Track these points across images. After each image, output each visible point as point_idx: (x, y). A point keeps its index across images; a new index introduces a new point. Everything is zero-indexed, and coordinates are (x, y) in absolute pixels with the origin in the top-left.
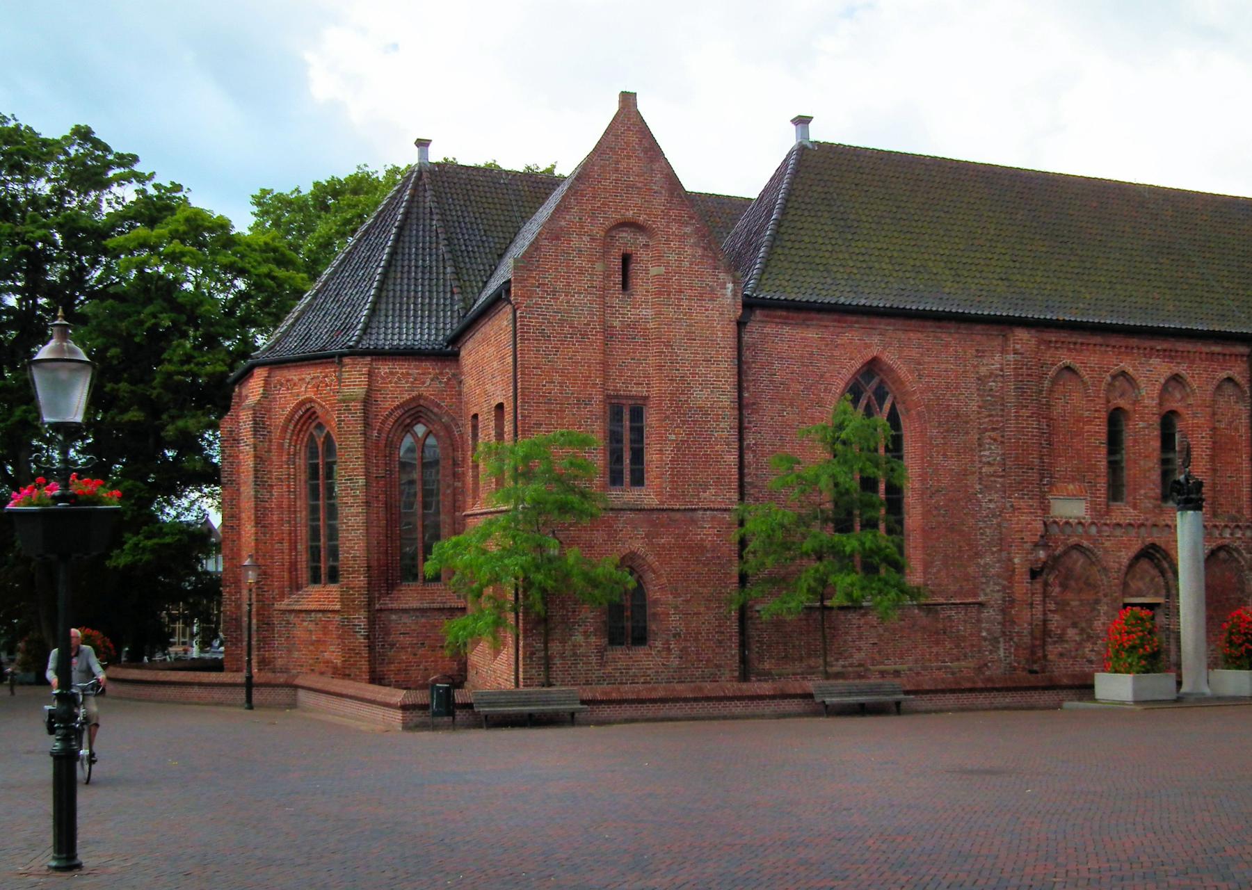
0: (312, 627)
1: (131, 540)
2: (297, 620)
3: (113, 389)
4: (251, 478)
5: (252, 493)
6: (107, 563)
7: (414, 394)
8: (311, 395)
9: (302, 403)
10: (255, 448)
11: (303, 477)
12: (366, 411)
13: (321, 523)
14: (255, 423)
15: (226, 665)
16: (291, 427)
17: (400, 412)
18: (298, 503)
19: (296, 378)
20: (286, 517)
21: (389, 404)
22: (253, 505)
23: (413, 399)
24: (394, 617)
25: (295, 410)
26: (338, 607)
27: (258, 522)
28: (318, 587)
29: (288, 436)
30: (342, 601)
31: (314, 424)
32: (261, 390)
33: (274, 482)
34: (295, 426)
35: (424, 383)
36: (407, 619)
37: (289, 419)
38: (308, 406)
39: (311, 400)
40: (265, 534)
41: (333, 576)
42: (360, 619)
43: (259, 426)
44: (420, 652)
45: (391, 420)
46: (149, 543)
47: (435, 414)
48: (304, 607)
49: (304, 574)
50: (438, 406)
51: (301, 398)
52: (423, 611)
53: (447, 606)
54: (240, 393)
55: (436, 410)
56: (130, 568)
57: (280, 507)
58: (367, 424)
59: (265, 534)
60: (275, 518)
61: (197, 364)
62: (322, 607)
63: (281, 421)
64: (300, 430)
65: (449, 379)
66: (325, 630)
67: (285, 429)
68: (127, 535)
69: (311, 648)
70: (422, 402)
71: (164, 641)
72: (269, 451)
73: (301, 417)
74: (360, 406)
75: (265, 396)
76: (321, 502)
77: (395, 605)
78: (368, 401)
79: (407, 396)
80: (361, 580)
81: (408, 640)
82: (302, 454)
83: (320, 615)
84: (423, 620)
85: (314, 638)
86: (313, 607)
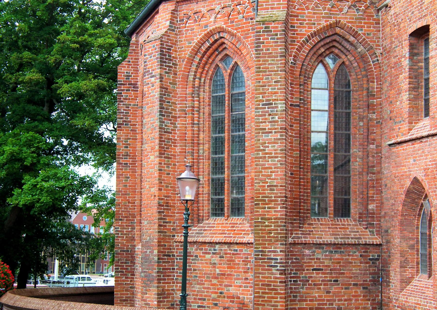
0: (216, 259)
1: (29, 181)
2: (200, 253)
3: (18, 58)
4: (157, 108)
5: (157, 123)
6: (8, 200)
7: (332, 21)
8: (221, 24)
9: (210, 34)
10: (161, 78)
11: (207, 110)
12: (286, 30)
13: (226, 155)
14: (162, 54)
15: (117, 295)
16: (197, 59)
17: (316, 39)
18: (202, 136)
19: (204, 10)
20: (188, 148)
21: (305, 31)
22: (157, 135)
23: (331, 26)
24: (307, 252)
25: (201, 43)
26: (250, 238)
27: (163, 151)
28: (220, 220)
29: (194, 68)
30: (256, 234)
31: (220, 57)
32: (168, 23)
33: (178, 113)
34: (201, 60)
35: (341, 10)
36: (320, 254)
37: (195, 52)
38: (216, 37)
39: (221, 30)
40: (168, 165)
41: (237, 209)
42: (277, 252)
43: (166, 56)
44: (333, 289)
45: (306, 48)
46: (46, 185)
47: (352, 44)
48: (208, 240)
49: (206, 207)
50: (356, 35)
51: (210, 28)
52: (337, 246)
53: (362, 241)
54: (137, 41)
55: (352, 39)
56: (29, 207)
57: (183, 138)
58: (287, 44)
59: (168, 165)
60: (178, 149)
61: (91, 35)
62: (228, 240)
63: (187, 53)
64: (206, 63)
65: (367, 8)
66: (231, 264)
67: (190, 61)
68: (27, 177)
69: (215, 281)
70: (338, 30)
71: (43, 269)
72: (174, 83)
73: (208, 49)
74: (280, 27)
75: (172, 28)
76: (226, 135)
77: (309, 240)
78: (288, 25)
79: (323, 23)
80: (278, 211)
81: (319, 277)
82: (207, 88)
83: (226, 247)
84: (337, 256)
85: (218, 271)
86: (217, 240)
